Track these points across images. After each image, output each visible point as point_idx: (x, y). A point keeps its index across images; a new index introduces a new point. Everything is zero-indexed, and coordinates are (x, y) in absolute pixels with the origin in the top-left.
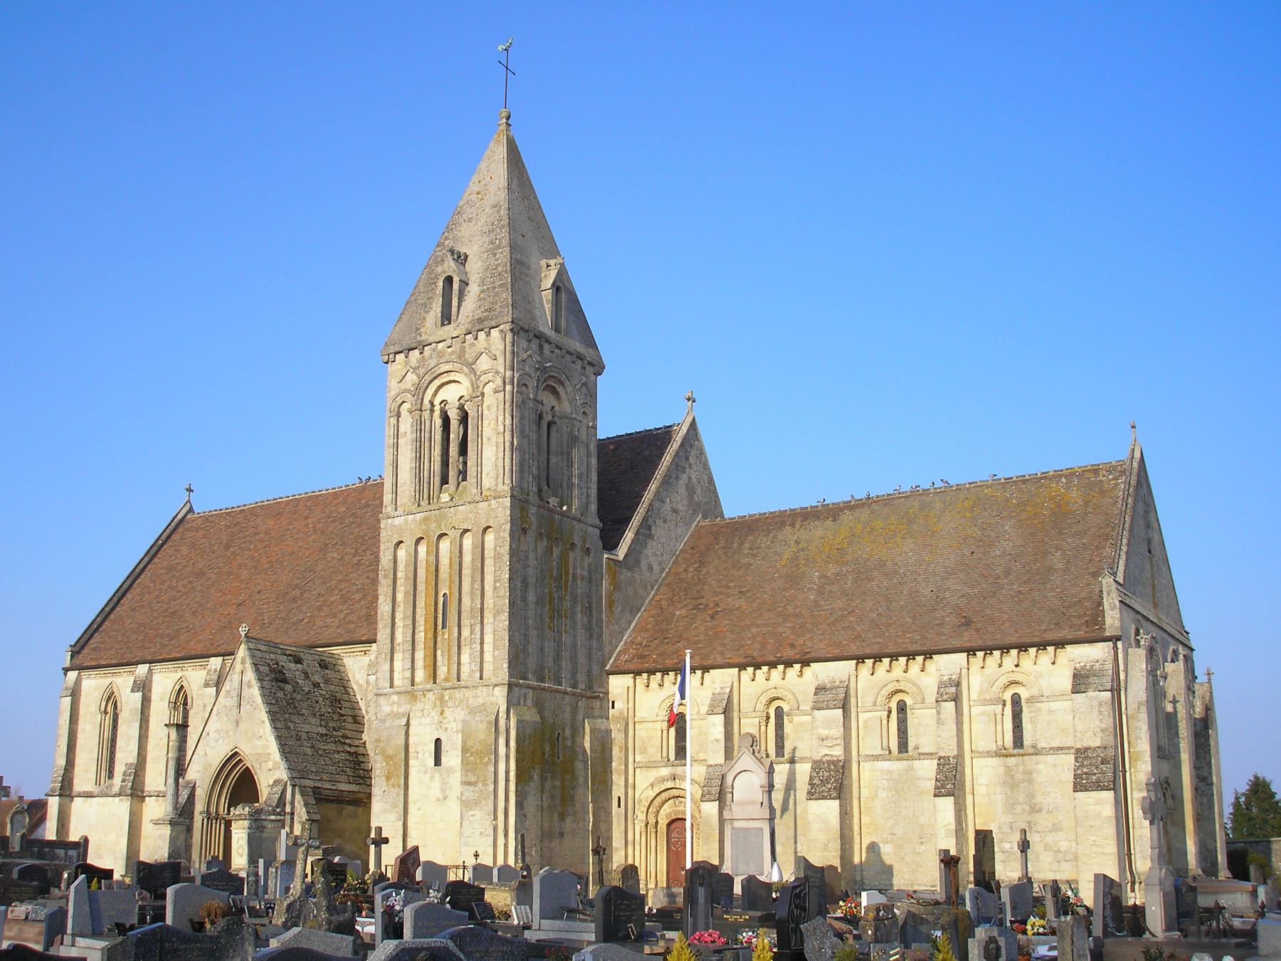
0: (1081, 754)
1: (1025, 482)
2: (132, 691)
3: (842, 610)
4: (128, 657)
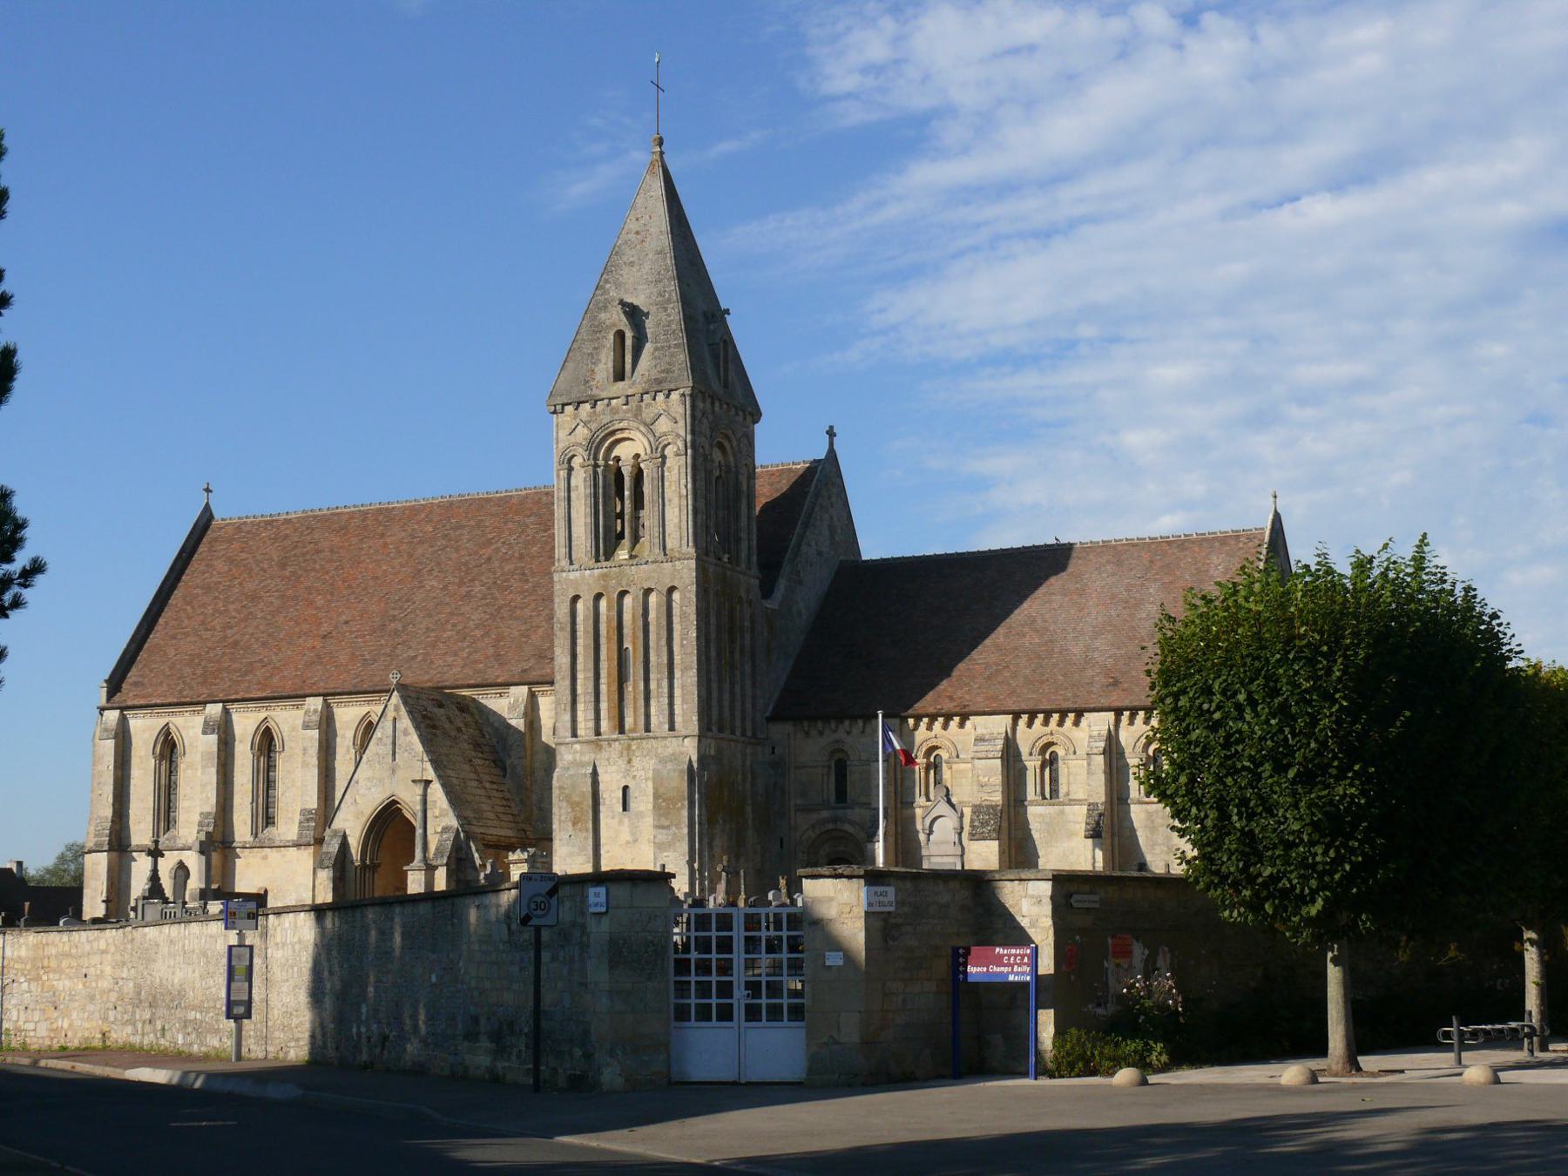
0: (319, 911)
1: (1169, 543)
2: (204, 733)
3: (997, 664)
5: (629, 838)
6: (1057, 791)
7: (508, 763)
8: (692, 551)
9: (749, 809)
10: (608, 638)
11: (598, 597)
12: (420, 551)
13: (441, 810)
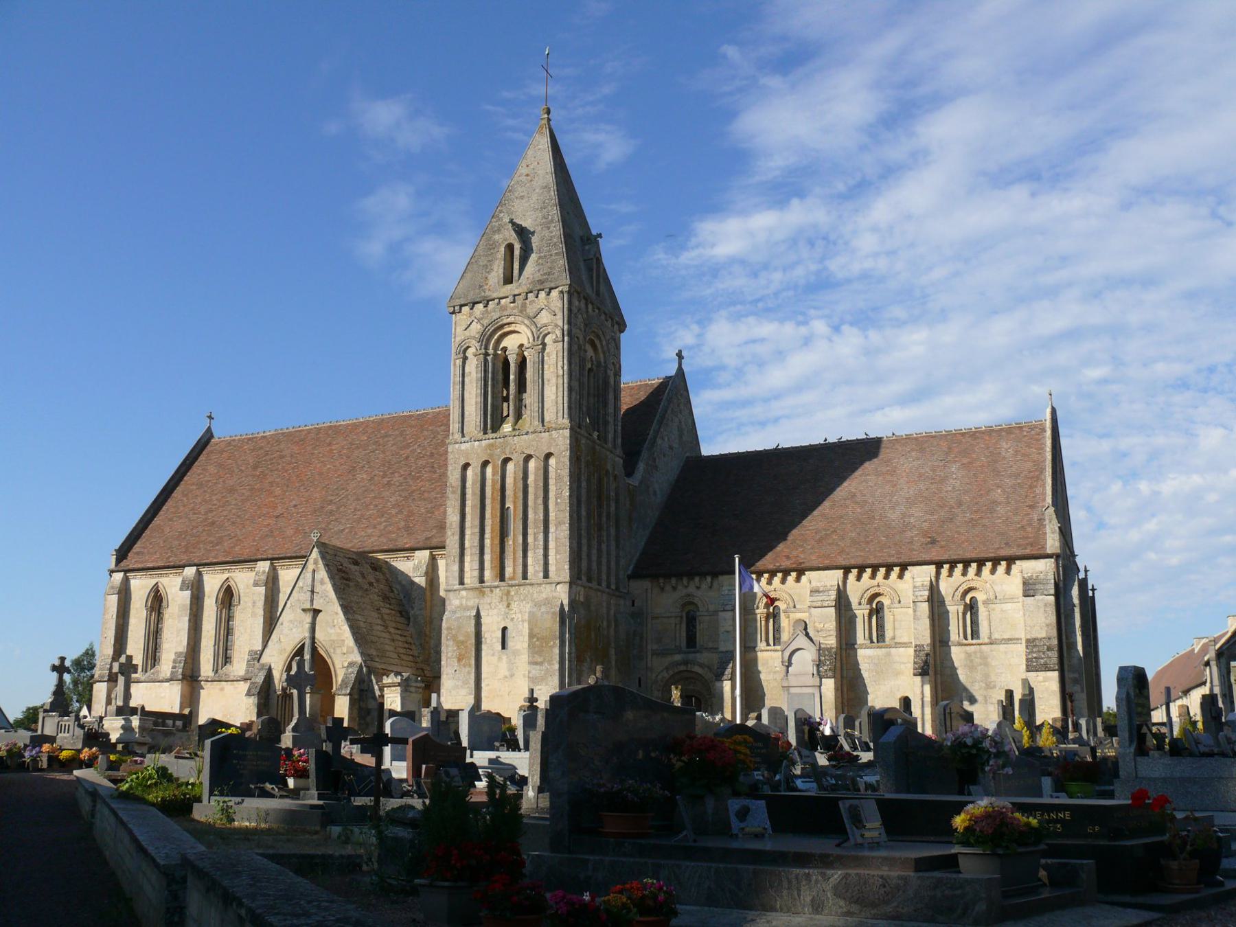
1: (963, 434)
2: (181, 589)
4: (173, 560)
5: (507, 674)
6: (883, 636)
7: (412, 613)
8: (567, 422)
9: (612, 652)
10: (493, 499)
11: (485, 464)
12: (356, 453)
13: (348, 647)
